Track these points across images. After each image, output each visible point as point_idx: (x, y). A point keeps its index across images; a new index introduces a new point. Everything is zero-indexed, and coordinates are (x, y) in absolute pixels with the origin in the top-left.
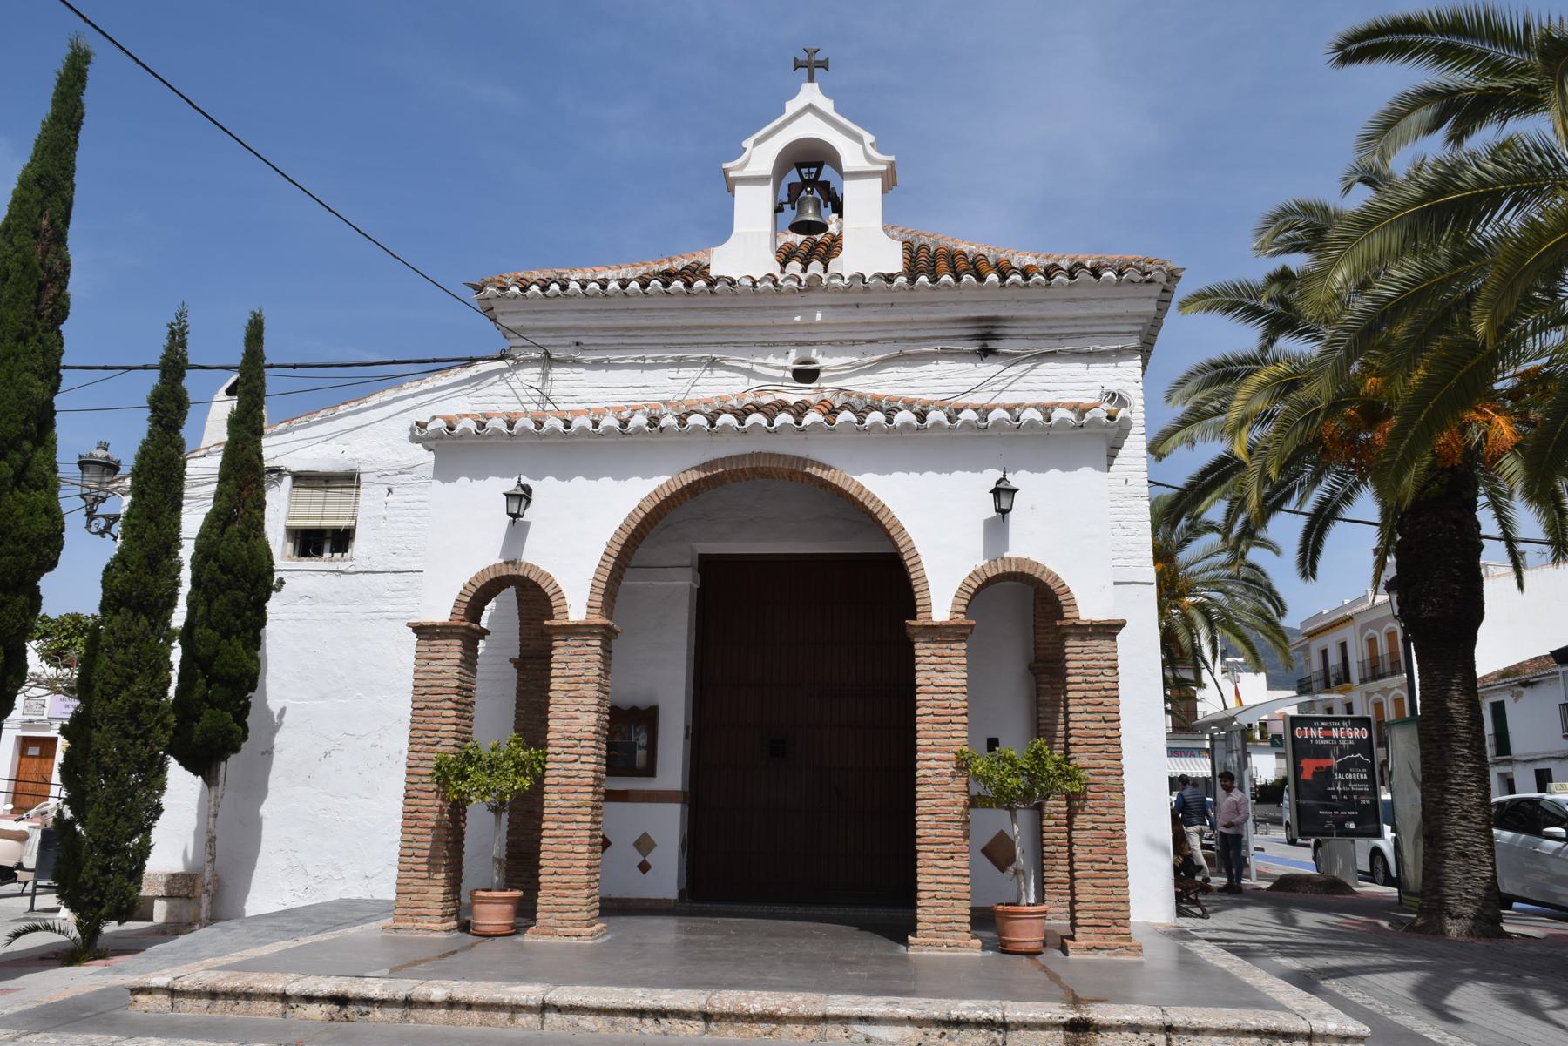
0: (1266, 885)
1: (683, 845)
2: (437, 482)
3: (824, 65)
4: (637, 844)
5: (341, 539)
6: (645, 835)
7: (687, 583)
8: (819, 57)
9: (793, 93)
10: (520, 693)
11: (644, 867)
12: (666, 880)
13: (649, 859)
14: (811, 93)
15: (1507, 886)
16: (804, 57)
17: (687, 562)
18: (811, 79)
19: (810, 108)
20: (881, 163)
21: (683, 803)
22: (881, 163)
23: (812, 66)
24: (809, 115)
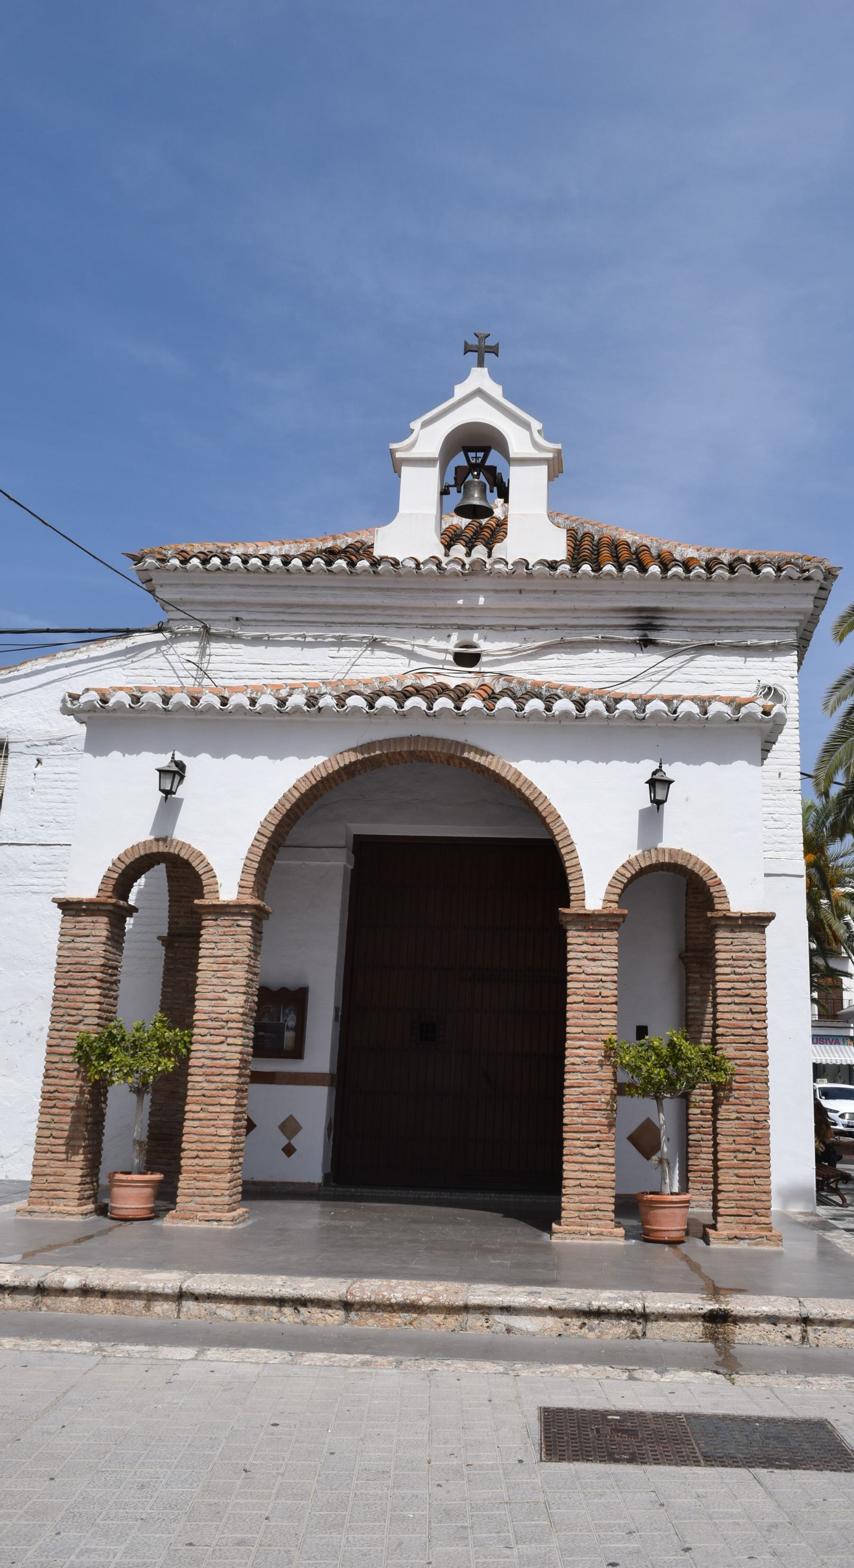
1: (329, 1129)
3: (494, 350)
8: (489, 342)
9: (463, 376)
11: (289, 1150)
12: (311, 1162)
13: (294, 1142)
14: (479, 378)
16: (474, 341)
17: (342, 843)
18: (481, 364)
19: (479, 392)
21: (331, 1085)
23: (482, 351)
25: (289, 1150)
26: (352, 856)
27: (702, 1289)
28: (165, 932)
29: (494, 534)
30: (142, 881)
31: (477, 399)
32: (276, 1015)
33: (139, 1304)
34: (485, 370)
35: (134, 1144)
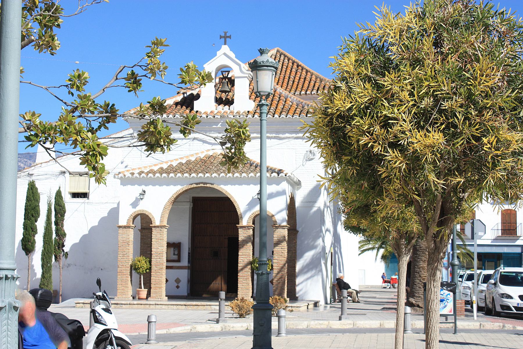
0: (204, 296)
1: (188, 281)
2: (122, 186)
3: (230, 37)
4: (176, 281)
5: (84, 195)
6: (178, 278)
7: (188, 207)
8: (228, 35)
9: (219, 49)
10: (141, 239)
11: (178, 287)
12: (184, 289)
13: (179, 285)
14: (225, 49)
15: (493, 286)
16: (223, 35)
17: (188, 200)
18: (225, 44)
19: (225, 54)
20: (247, 74)
21: (188, 269)
22: (247, 74)
23: (225, 38)
24: (224, 57)
25: (178, 287)
26: (192, 204)
27: (174, 140)
28: (140, 228)
29: (229, 102)
30: (39, 275)
31: (224, 57)
32: (174, 246)
33: (148, 306)
34: (226, 46)
35: (233, 100)
